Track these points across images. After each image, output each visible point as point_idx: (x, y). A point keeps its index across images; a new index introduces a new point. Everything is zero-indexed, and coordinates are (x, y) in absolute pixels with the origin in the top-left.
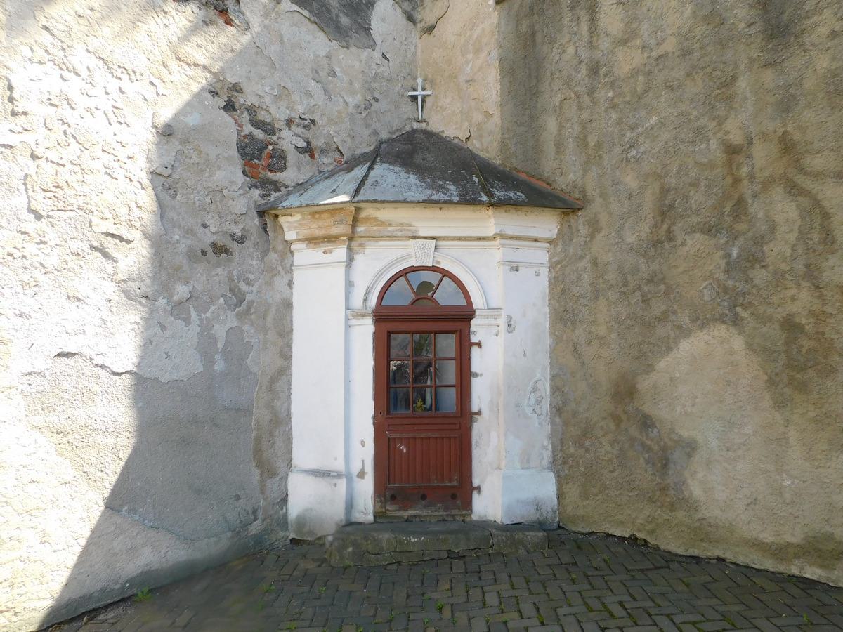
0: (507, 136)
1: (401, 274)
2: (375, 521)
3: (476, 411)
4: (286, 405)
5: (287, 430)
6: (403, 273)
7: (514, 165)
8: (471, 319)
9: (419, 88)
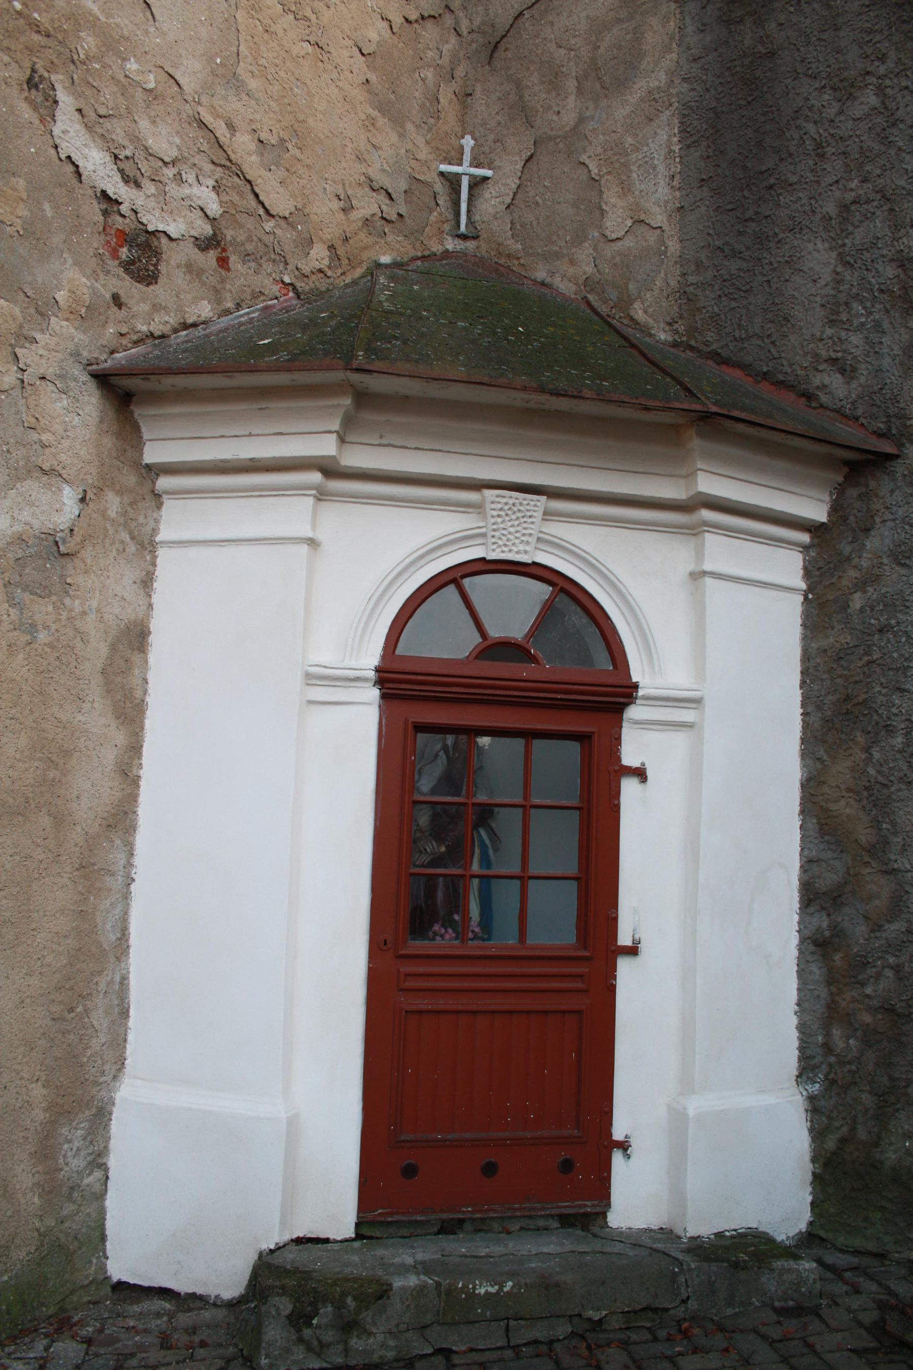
0: (692, 279)
1: (555, 579)
2: (359, 1236)
3: (629, 943)
4: (118, 911)
5: (118, 978)
6: (562, 583)
7: (714, 347)
8: (627, 705)
9: (467, 157)
